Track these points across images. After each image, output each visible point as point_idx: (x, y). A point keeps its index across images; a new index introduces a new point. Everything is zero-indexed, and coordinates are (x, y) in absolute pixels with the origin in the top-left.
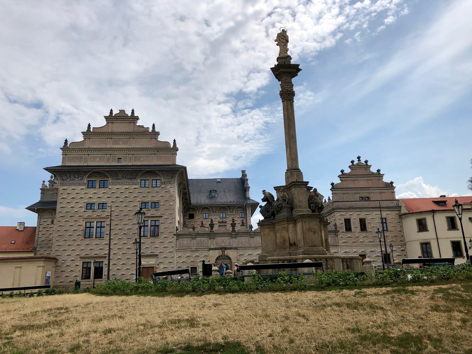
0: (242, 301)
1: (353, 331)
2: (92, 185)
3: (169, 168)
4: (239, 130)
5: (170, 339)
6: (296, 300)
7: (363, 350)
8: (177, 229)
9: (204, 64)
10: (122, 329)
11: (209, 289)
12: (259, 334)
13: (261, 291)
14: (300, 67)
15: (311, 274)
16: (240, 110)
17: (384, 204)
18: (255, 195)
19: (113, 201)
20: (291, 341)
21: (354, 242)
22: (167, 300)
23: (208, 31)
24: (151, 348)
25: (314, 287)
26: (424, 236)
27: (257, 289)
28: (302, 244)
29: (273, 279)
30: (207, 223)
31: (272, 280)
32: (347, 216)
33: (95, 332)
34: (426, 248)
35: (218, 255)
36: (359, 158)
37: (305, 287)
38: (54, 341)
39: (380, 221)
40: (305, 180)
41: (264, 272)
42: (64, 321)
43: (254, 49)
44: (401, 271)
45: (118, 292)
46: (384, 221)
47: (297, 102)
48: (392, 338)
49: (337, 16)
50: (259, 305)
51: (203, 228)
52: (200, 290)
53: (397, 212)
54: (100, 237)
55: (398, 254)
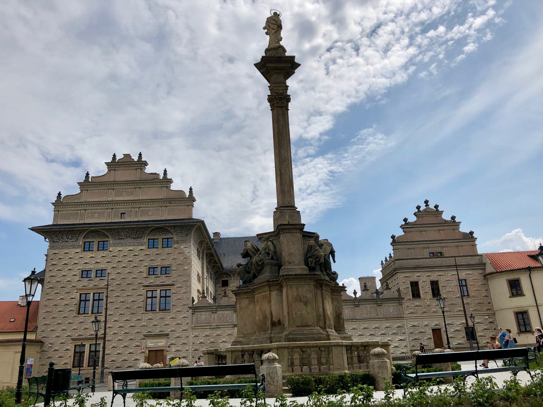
2: (103, 247)
16: (300, 159)
17: (460, 261)
26: (519, 303)
34: (523, 319)
36: (426, 202)
39: (457, 283)
43: (313, 89)
46: (463, 284)
49: (408, 47)
53: (481, 272)
55: (485, 327)
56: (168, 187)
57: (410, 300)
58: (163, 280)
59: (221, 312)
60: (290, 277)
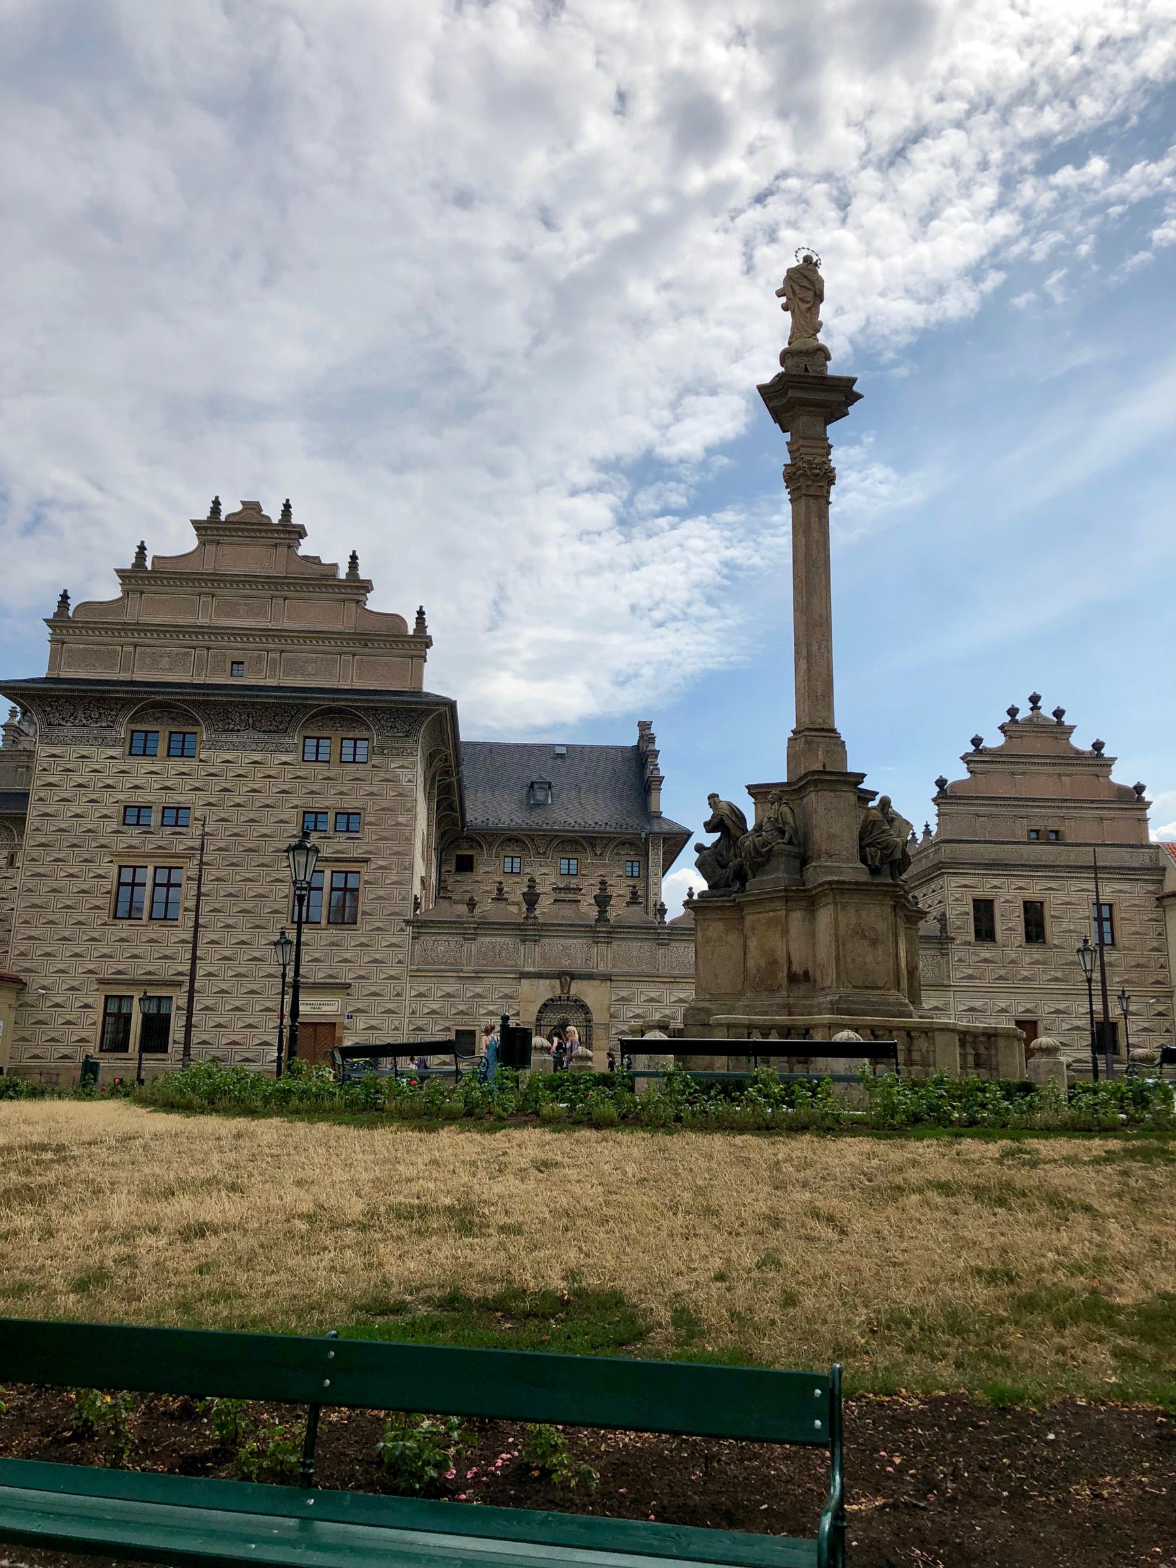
0: (627, 1157)
1: (992, 1277)
4: (636, 586)
5: (392, 1268)
6: (807, 1165)
7: (1023, 1344)
8: (417, 905)
9: (528, 355)
10: (240, 1227)
11: (520, 1110)
12: (684, 1268)
13: (693, 1128)
14: (856, 388)
15: (858, 1080)
16: (642, 518)
17: (1108, 857)
18: (683, 805)
19: (212, 800)
20: (790, 1300)
21: (1001, 978)
22: (383, 1138)
23: (548, 245)
24: (331, 1294)
25: (866, 1124)
27: (678, 1119)
28: (830, 978)
29: (732, 1088)
30: (516, 890)
31: (724, 1090)
32: (984, 891)
33: (154, 1230)
35: (550, 996)
36: (1035, 699)
37: (837, 1121)
38: (22, 1253)
40: (852, 767)
41: (700, 1062)
42: (52, 1189)
43: (700, 312)
44: (1156, 1085)
45: (224, 1103)
46: (1104, 915)
47: (842, 501)
48: (1120, 1309)
49: (992, 211)
50: (684, 1174)
51: (502, 905)
52: (490, 1113)
53: (1151, 887)
54: (165, 918)
55: (1146, 1025)
56: (360, 603)
57: (969, 944)
59: (487, 939)
60: (847, 887)
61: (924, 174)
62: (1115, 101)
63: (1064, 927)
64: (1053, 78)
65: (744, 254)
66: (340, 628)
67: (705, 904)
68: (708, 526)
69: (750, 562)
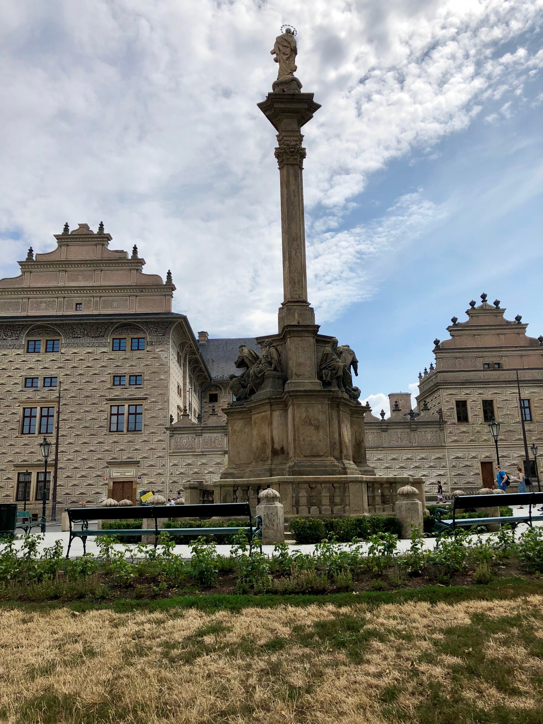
3: (158, 318)
16: (318, 234)
19: (68, 373)
21: (472, 441)
36: (484, 297)
39: (517, 404)
43: (338, 136)
49: (473, 78)
56: (139, 270)
57: (455, 424)
58: (132, 392)
59: (208, 435)
60: (298, 394)
61: (439, 63)
62: (527, 21)
63: (505, 412)
64: (497, 13)
65: (357, 108)
66: (129, 283)
67: (232, 410)
68: (348, 236)
69: (369, 251)
